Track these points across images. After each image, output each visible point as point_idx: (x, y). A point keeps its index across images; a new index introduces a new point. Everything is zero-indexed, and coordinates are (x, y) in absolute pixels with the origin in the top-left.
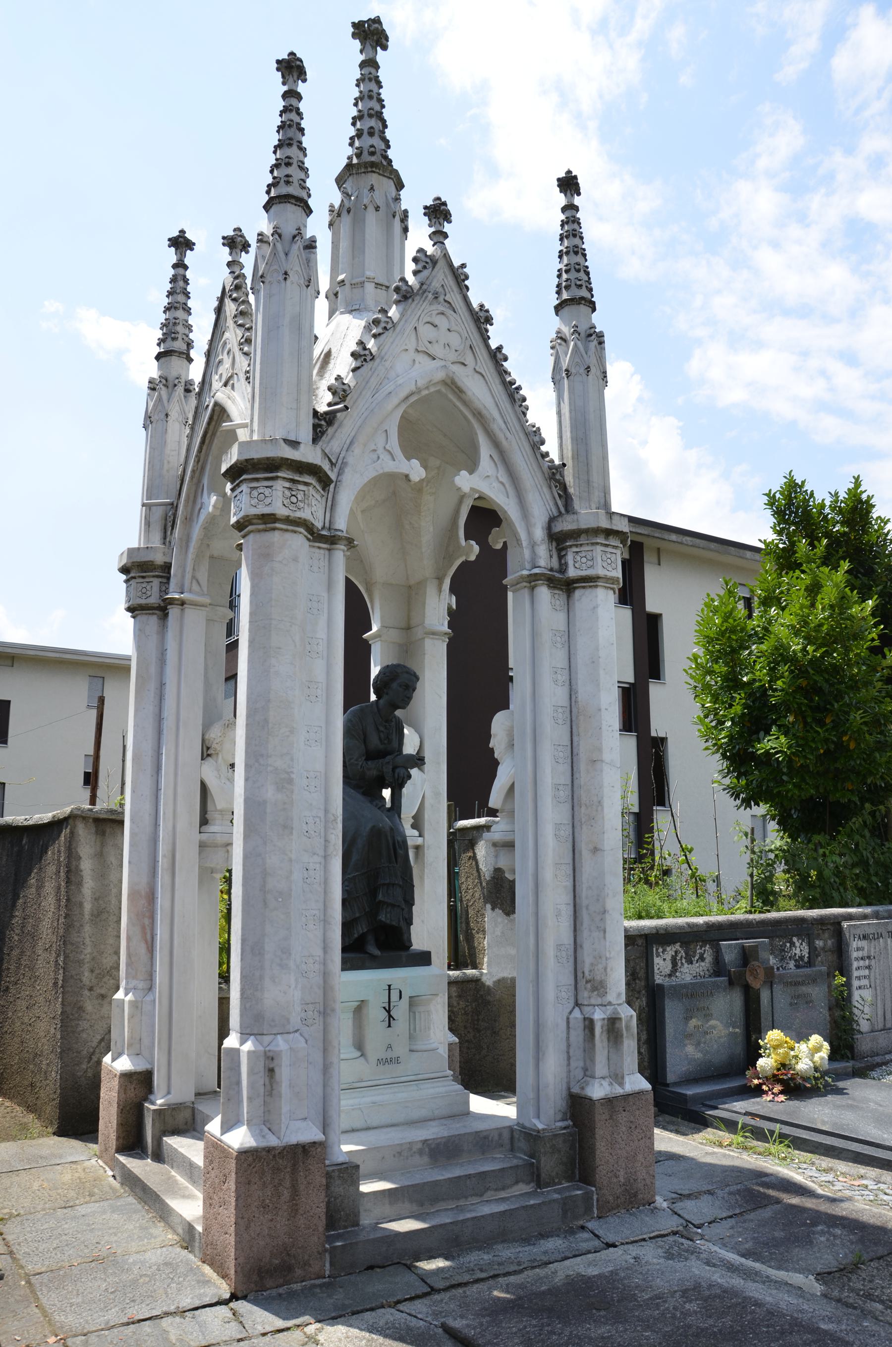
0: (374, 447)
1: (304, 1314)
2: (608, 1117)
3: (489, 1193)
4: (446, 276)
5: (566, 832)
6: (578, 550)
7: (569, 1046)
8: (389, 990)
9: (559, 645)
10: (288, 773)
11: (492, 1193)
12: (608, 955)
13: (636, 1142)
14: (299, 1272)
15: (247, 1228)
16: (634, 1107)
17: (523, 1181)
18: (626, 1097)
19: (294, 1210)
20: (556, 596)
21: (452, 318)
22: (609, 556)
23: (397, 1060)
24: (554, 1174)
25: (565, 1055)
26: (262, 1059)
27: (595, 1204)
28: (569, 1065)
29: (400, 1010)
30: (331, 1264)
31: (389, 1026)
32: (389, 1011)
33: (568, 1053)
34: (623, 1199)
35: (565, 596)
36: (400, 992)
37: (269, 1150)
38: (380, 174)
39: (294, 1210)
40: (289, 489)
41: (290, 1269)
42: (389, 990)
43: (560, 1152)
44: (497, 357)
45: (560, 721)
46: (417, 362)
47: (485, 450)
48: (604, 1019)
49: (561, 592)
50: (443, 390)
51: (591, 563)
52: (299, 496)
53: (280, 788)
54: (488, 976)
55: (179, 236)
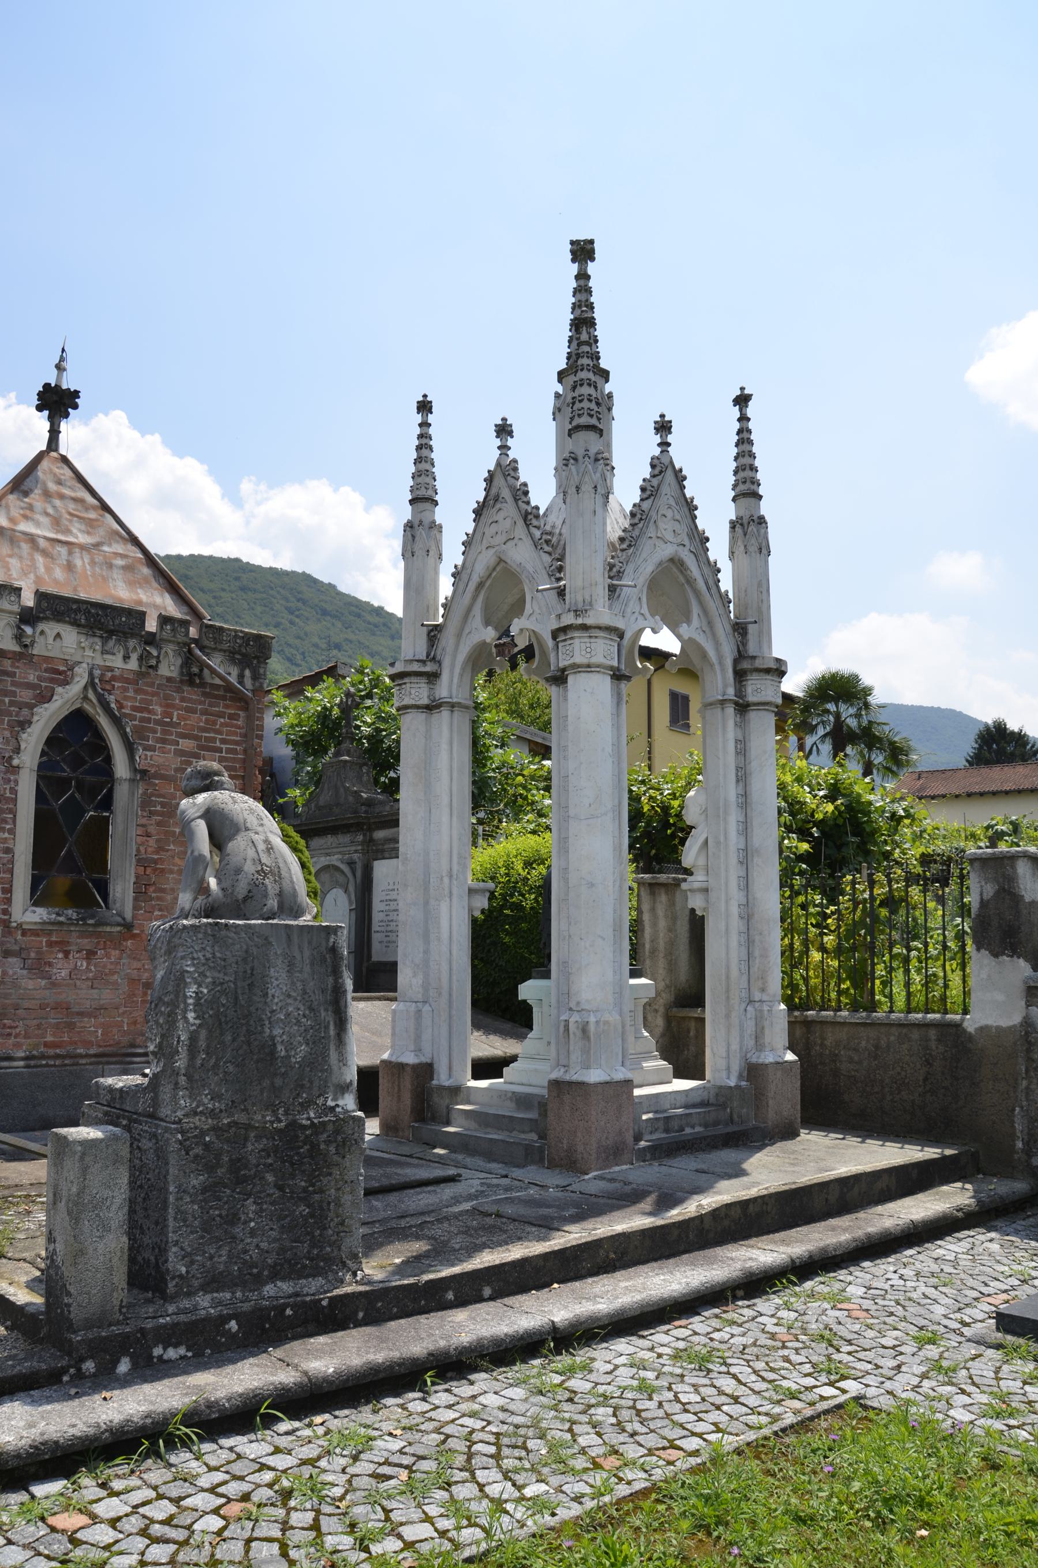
18: (570, 1083)
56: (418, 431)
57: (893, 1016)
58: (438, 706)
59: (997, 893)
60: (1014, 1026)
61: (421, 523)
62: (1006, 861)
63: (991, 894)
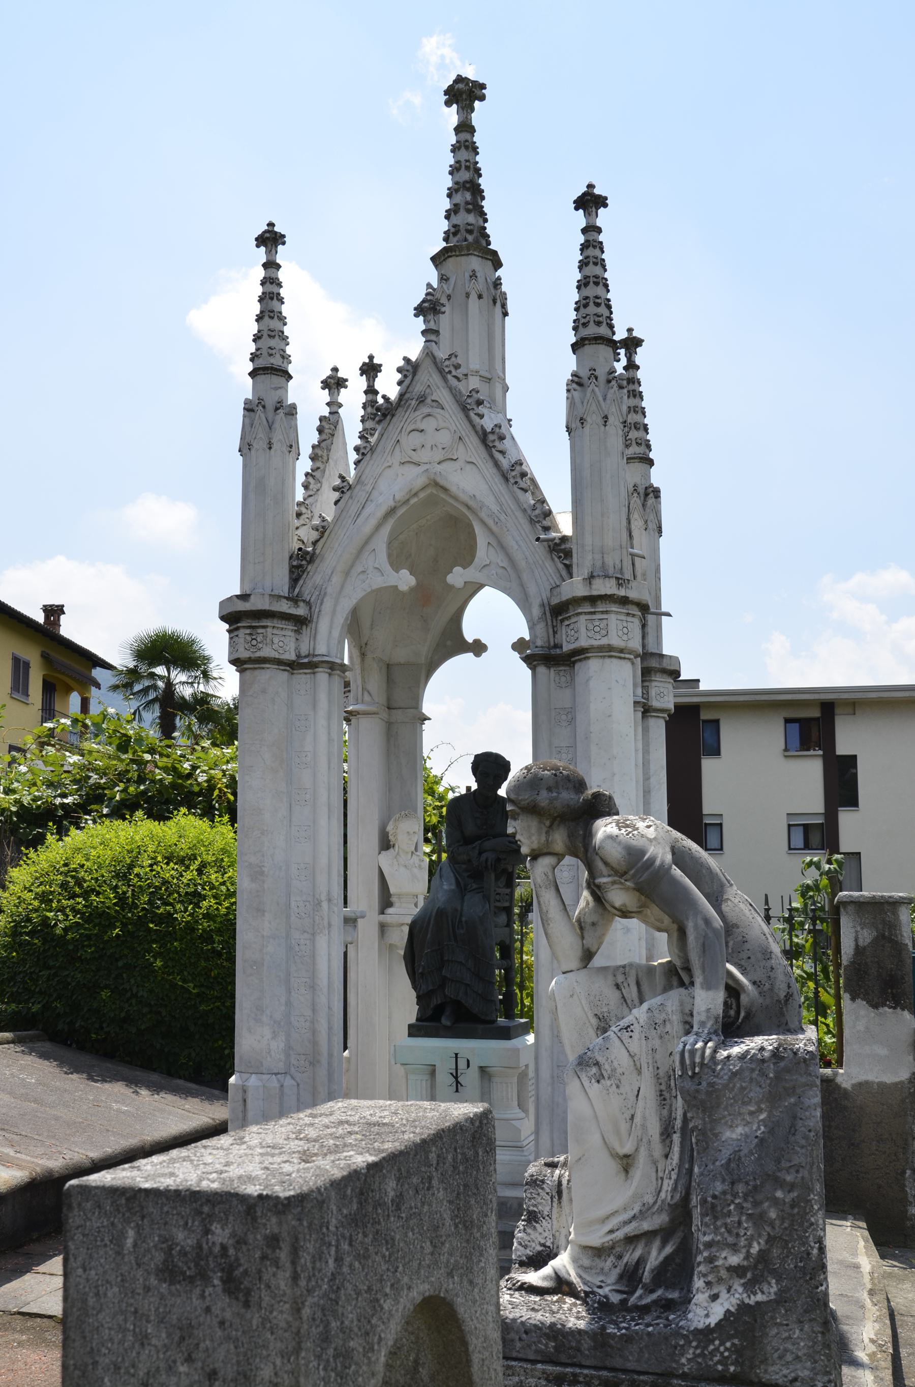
0: (361, 569)
9: (564, 724)
21: (438, 416)
22: (597, 623)
26: (241, 1091)
31: (457, 1091)
32: (456, 1078)
36: (468, 1061)
38: (457, 256)
40: (251, 634)
46: (400, 475)
47: (482, 539)
49: (567, 668)
50: (435, 492)
51: (576, 635)
52: (259, 640)
54: (845, 1077)
55: (584, 194)
59: (875, 941)
60: (901, 1082)
62: (886, 907)
63: (868, 941)
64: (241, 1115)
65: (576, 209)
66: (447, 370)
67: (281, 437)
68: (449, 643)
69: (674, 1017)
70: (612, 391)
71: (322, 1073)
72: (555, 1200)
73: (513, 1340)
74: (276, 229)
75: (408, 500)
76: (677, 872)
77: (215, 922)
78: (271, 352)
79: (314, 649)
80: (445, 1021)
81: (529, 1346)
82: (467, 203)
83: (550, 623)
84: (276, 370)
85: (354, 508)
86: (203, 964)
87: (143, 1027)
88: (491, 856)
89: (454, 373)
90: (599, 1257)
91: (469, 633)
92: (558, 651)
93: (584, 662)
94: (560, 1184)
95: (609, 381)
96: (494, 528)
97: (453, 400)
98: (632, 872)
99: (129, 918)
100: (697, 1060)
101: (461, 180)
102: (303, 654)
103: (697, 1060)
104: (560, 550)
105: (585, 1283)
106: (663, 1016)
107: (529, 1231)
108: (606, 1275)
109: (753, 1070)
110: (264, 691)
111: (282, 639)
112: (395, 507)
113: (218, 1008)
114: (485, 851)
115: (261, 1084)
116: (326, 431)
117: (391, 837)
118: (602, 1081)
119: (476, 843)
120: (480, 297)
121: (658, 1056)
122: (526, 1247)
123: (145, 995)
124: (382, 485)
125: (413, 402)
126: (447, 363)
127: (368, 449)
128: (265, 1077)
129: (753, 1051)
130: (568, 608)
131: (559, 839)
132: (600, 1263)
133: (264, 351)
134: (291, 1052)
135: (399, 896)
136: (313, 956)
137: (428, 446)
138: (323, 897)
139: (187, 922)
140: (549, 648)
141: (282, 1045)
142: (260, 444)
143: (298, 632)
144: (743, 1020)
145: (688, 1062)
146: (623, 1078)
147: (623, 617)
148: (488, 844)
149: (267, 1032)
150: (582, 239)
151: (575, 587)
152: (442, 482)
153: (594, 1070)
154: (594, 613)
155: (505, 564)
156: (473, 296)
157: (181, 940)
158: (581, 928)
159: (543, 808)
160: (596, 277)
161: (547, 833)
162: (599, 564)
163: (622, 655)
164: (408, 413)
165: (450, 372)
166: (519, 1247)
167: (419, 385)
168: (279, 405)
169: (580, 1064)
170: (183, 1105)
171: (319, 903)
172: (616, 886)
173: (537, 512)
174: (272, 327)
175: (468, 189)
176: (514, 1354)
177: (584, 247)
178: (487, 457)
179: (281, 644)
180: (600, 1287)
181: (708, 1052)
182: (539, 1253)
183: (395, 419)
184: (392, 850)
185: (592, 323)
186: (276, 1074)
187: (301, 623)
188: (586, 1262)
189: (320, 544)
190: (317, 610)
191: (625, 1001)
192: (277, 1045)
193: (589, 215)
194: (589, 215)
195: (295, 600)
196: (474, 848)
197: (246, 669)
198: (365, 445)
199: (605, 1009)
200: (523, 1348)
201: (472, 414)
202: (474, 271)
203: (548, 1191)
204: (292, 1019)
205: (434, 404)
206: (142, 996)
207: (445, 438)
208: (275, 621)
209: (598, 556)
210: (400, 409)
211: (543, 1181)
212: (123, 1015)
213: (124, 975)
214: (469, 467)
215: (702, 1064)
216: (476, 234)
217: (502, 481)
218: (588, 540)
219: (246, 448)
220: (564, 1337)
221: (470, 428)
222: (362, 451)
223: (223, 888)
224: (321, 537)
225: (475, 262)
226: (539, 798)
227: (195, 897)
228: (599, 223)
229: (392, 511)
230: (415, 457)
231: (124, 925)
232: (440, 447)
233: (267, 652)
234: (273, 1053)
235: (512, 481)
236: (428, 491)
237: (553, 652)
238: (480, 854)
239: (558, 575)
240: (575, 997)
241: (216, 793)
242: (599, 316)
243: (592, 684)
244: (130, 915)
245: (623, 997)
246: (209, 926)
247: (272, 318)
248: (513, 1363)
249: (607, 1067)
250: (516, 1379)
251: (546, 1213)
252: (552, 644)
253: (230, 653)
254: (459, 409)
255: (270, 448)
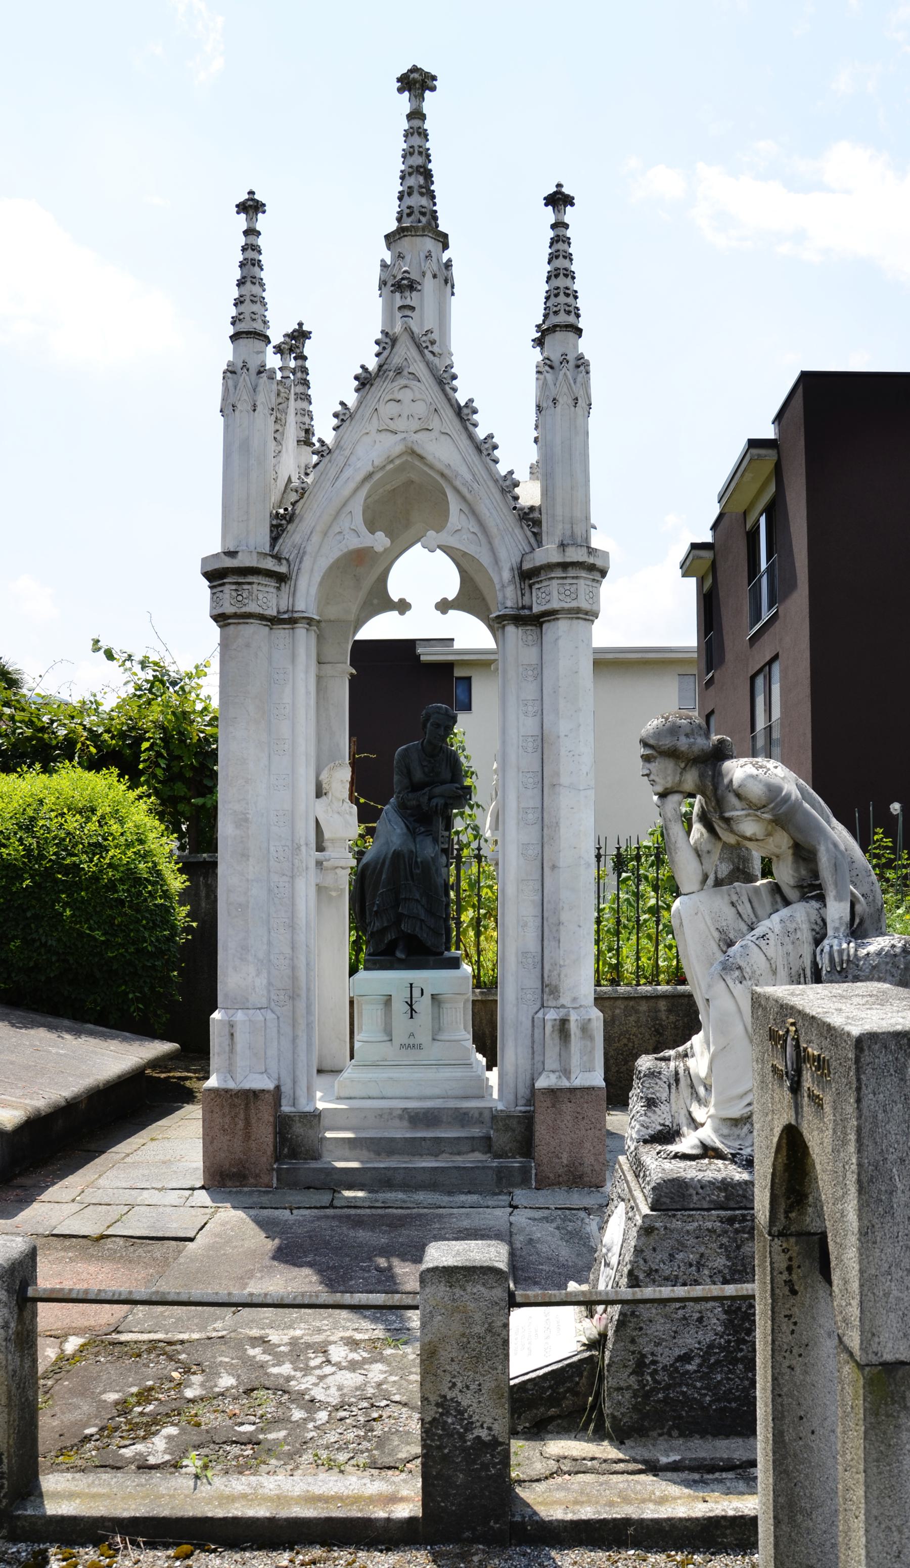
0: (339, 530)
1: (227, 1202)
2: (550, 1105)
3: (444, 1155)
4: (408, 349)
5: (534, 851)
6: (539, 586)
7: (533, 1042)
8: (411, 987)
9: (531, 679)
10: (244, 814)
11: (448, 1155)
12: (562, 963)
13: (583, 1132)
14: (252, 1181)
15: (212, 1142)
16: (582, 1100)
17: (480, 1151)
18: (572, 1090)
19: (247, 1137)
20: (529, 632)
22: (568, 588)
23: (420, 1047)
24: (507, 1148)
25: (530, 1051)
26: (227, 1026)
27: (533, 1176)
28: (533, 1058)
29: (423, 1005)
30: (278, 1180)
31: (412, 1017)
32: (411, 1005)
33: (533, 1048)
34: (565, 1178)
35: (539, 630)
36: (422, 990)
37: (227, 1091)
39: (247, 1137)
40: (236, 590)
41: (245, 1177)
42: (411, 987)
43: (514, 1131)
44: (464, 414)
45: (530, 750)
46: (377, 442)
48: (555, 1020)
49: (534, 628)
50: (409, 459)
51: (548, 598)
52: (244, 596)
53: (238, 826)
55: (555, 193)
56: (242, 240)
57: (622, 989)
58: (292, 621)
61: (245, 366)
63: (726, 873)
64: (227, 1049)
65: (546, 205)
66: (424, 345)
67: (264, 400)
68: (375, 601)
69: (804, 926)
70: (581, 375)
71: (301, 1005)
72: (673, 1087)
73: (691, 1195)
74: (256, 197)
75: (384, 466)
76: (806, 805)
77: (118, 871)
78: (254, 317)
79: (293, 606)
80: (400, 955)
81: (704, 1198)
82: (421, 187)
83: (518, 586)
84: (259, 335)
85: (333, 472)
86: (109, 912)
87: (52, 975)
88: (441, 801)
89: (430, 349)
90: (736, 1126)
91: (395, 592)
92: (527, 612)
93: (553, 623)
94: (677, 1073)
95: (578, 366)
96: (468, 496)
97: (430, 374)
98: (772, 805)
99: (36, 870)
100: (845, 958)
101: (415, 165)
102: (282, 611)
103: (845, 958)
104: (530, 519)
105: (729, 1147)
106: (794, 925)
107: (649, 1114)
108: (743, 1139)
109: (887, 963)
110: (248, 645)
111: (266, 595)
112: (373, 473)
113: (121, 954)
114: (433, 797)
115: (246, 1018)
116: (282, 395)
117: (324, 786)
118: (744, 982)
119: (426, 789)
120: (435, 276)
121: (791, 959)
122: (647, 1128)
123: (54, 943)
124: (360, 450)
125: (391, 373)
126: (424, 338)
127: (347, 416)
128: (251, 1012)
129: (887, 949)
130: (540, 573)
131: (690, 780)
132: (736, 1131)
133: (247, 316)
134: (271, 988)
135: (333, 841)
136: (293, 897)
137: (405, 416)
138: (302, 842)
139: (93, 872)
140: (518, 609)
141: (265, 982)
142: (243, 406)
143: (278, 589)
144: (858, 926)
145: (837, 960)
146: (761, 978)
147: (589, 583)
148: (438, 790)
149: (252, 970)
150: (551, 234)
151: (548, 553)
152: (419, 451)
153: (737, 973)
154: (565, 578)
155: (476, 529)
156: (429, 275)
157: (86, 890)
158: (699, 856)
159: (682, 752)
160: (566, 269)
161: (681, 774)
162: (568, 533)
163: (587, 617)
164: (386, 383)
165: (427, 347)
166: (642, 1128)
167: (396, 357)
168: (262, 369)
169: (724, 969)
170: (108, 1047)
171: (299, 847)
172: (749, 818)
173: (508, 483)
174: (253, 293)
175: (421, 174)
176: (692, 1206)
177: (554, 241)
178: (462, 430)
179: (265, 600)
180: (741, 1149)
181: (852, 951)
182: (660, 1131)
183: (373, 388)
184: (324, 797)
185: (562, 311)
186: (260, 1009)
187: (281, 579)
188: (726, 1131)
189: (300, 504)
190: (296, 568)
191: (740, 916)
192: (261, 982)
193: (559, 211)
194: (559, 211)
195: (278, 558)
196: (424, 794)
197: (230, 624)
198: (345, 411)
199: (724, 924)
200: (699, 1200)
201: (447, 388)
202: (429, 251)
203: (665, 1080)
204: (272, 957)
205: (410, 376)
206: (51, 945)
207: (420, 409)
208: (260, 578)
209: (568, 526)
210: (378, 379)
211: (660, 1073)
212: (31, 964)
213: (33, 926)
214: (443, 437)
215: (848, 961)
216: (428, 216)
217: (475, 452)
218: (559, 511)
219: (228, 408)
220: (733, 1188)
221: (446, 401)
222: (341, 417)
223: (122, 839)
224: (301, 498)
225: (429, 244)
226: (679, 743)
227: (98, 848)
228: (567, 220)
229: (370, 476)
230: (392, 426)
231: (32, 877)
232: (416, 417)
233: (252, 608)
234: (257, 990)
235: (485, 453)
236: (404, 458)
237: (523, 612)
238: (430, 799)
239: (526, 542)
240: (699, 914)
241: (79, 746)
242: (569, 306)
243: (561, 643)
244: (37, 866)
245: (739, 913)
246: (113, 876)
247: (254, 283)
248: (692, 1213)
249: (748, 970)
250: (696, 1224)
251: (664, 1098)
252: (520, 605)
253: (212, 608)
254: (435, 382)
255: (254, 410)
